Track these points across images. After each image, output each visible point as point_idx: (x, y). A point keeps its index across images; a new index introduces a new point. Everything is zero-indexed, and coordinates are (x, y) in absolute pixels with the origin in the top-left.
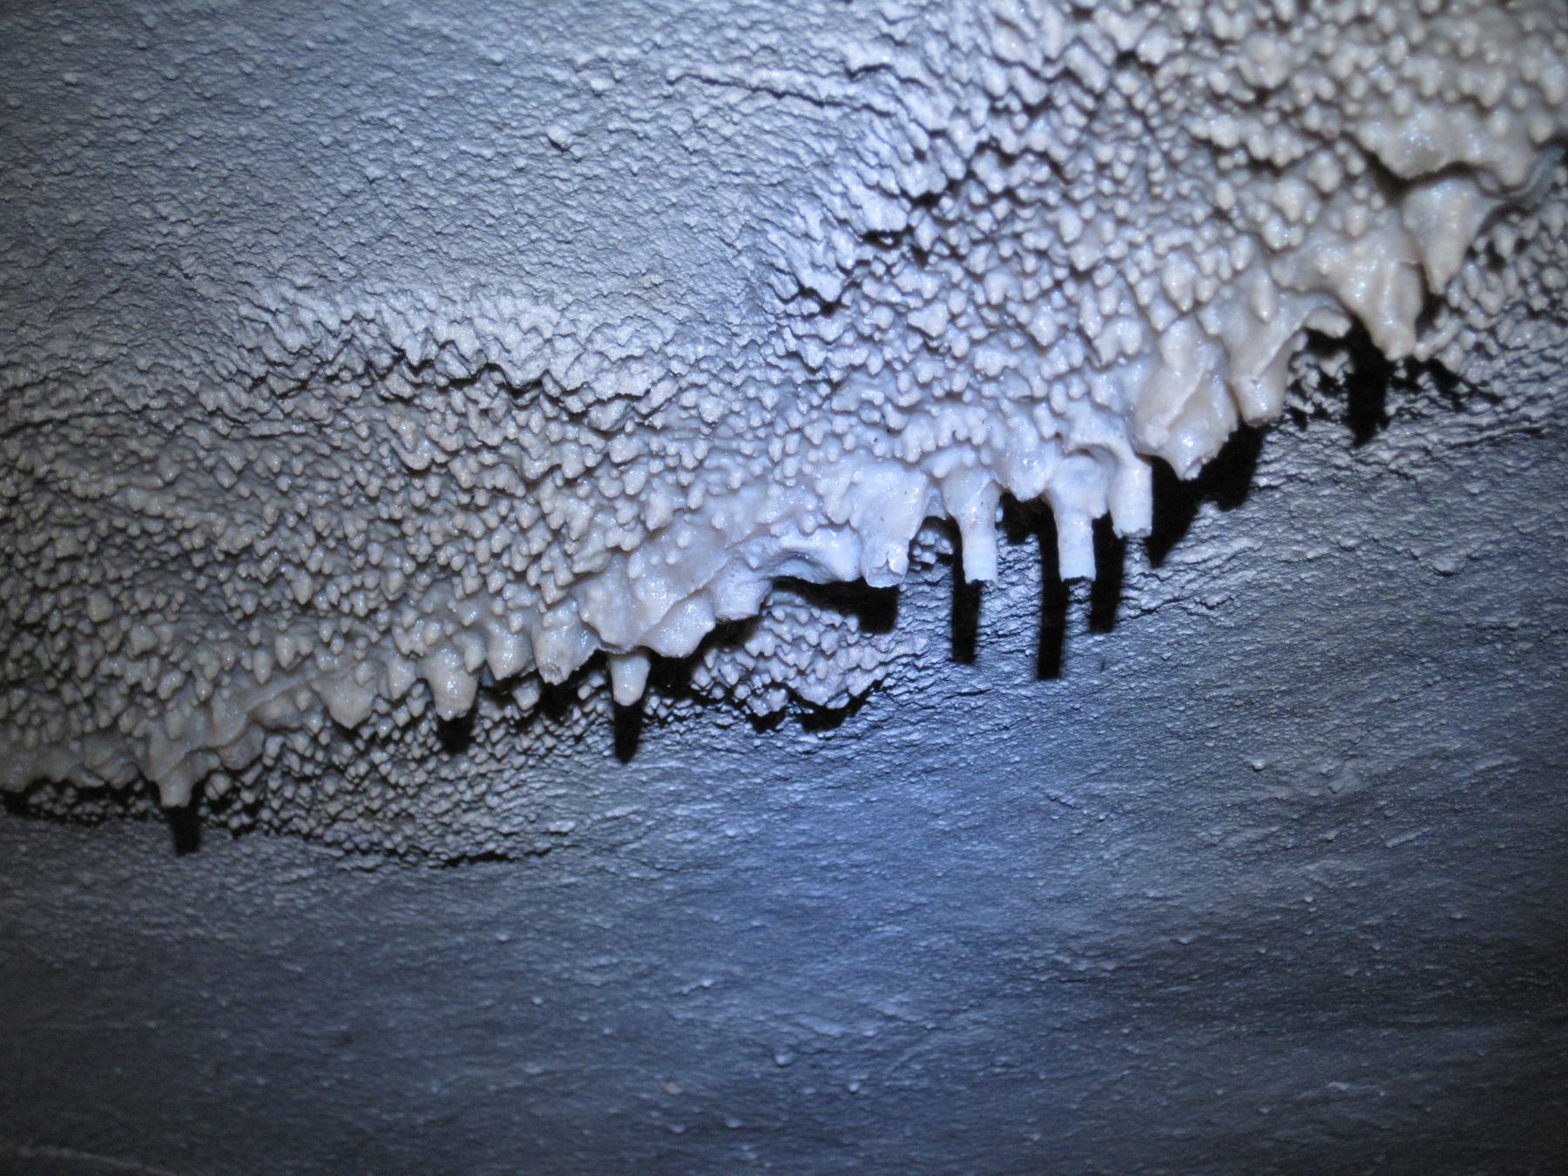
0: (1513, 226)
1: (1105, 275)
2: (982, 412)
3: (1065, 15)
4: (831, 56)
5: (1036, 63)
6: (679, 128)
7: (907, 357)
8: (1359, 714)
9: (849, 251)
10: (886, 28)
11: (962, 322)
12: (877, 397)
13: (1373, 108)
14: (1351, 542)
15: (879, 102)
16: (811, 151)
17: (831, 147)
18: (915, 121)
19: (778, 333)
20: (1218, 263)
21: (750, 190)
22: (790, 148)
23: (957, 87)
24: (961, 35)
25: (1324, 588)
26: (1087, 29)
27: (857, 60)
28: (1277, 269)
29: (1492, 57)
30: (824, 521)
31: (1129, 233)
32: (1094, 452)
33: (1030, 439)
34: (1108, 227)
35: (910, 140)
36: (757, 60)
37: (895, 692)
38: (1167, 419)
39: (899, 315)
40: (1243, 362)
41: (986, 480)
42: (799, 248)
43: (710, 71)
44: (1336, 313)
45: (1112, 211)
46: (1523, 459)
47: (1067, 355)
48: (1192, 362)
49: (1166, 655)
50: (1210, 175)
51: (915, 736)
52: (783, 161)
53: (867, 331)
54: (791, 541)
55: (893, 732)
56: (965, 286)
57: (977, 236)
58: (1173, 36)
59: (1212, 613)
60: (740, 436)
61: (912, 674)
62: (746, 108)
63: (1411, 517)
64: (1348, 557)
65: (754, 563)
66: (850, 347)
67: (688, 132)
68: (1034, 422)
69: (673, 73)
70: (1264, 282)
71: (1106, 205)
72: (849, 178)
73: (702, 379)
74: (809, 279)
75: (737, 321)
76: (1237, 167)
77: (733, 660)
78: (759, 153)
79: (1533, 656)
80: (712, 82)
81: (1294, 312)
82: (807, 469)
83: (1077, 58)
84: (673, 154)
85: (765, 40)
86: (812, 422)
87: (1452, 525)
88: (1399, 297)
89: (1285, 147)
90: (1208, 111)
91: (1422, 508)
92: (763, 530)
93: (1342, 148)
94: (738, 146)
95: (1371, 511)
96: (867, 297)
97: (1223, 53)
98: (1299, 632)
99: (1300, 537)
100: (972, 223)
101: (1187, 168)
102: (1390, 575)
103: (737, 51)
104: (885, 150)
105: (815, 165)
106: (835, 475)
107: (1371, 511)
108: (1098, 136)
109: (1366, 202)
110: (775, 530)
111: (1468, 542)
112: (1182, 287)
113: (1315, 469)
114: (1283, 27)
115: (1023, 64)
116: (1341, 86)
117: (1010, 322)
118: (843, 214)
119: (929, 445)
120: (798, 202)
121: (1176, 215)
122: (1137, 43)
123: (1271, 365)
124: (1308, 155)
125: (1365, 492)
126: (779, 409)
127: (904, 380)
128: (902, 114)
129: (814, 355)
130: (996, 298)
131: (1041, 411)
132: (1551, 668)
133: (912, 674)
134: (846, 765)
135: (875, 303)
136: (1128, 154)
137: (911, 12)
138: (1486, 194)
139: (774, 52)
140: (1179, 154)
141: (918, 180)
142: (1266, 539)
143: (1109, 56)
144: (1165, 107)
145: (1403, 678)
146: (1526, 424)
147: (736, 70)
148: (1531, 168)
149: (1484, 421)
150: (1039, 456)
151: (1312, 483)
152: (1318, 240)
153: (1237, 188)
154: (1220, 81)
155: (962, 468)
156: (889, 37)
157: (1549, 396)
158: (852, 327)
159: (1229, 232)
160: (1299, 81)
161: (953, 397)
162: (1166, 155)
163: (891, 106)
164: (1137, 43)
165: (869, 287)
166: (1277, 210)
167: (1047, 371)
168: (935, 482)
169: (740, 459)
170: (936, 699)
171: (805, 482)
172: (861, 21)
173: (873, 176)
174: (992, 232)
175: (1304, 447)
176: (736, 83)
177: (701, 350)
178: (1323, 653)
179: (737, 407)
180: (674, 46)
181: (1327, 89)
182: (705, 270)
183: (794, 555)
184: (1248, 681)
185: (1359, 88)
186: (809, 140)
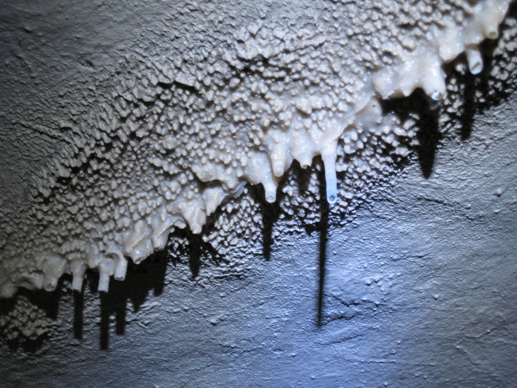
0: (232, 204)
1: (122, 202)
2: (84, 242)
3: (119, 119)
4: (56, 123)
5: (109, 131)
6: (13, 139)
7: (65, 220)
8: (187, 373)
9: (53, 183)
10: (71, 117)
11: (82, 212)
12: (56, 233)
13: (196, 161)
14: (186, 308)
15: (67, 139)
16: (47, 152)
17: (52, 151)
18: (75, 145)
19: (30, 208)
20: (153, 203)
21: (29, 162)
22: (42, 150)
23: (88, 136)
24: (90, 121)
25: (178, 323)
26: (123, 125)
27: (63, 124)
28: (168, 207)
29: (228, 151)
30: (35, 269)
31: (130, 191)
32: (114, 256)
33: (96, 252)
34: (124, 188)
35: (73, 150)
36: (36, 121)
37: (51, 339)
38: (133, 245)
39: (65, 207)
40: (156, 232)
41: (82, 263)
42: (40, 181)
43: (23, 122)
44: (182, 221)
45: (125, 183)
46: (236, 286)
47: (109, 226)
48: (142, 232)
49: (132, 340)
50: (153, 176)
51: (56, 359)
52: (39, 154)
53: (55, 210)
54: (25, 274)
55: (50, 356)
56: (84, 200)
57: (88, 184)
58: (147, 131)
59: (146, 327)
60: (15, 240)
61: (56, 333)
62: (32, 136)
63: (203, 302)
64: (185, 313)
65: (14, 280)
66: (50, 215)
67: (15, 141)
68: (98, 246)
69: (14, 121)
70: (164, 211)
71: (124, 181)
72: (56, 161)
73: (7, 219)
74: (41, 190)
75: (20, 202)
76: (160, 174)
77: (4, 318)
78: (33, 150)
79: (238, 360)
80: (23, 126)
81: (171, 220)
82: (33, 253)
83: (120, 132)
84: (10, 147)
85: (40, 115)
86: (37, 238)
87: (215, 307)
88: (199, 218)
89: (173, 170)
90: (154, 156)
91: (207, 299)
92: (18, 270)
93: (188, 172)
94: (28, 147)
95: (193, 298)
96: (57, 200)
97: (159, 139)
98: (171, 339)
99: (172, 304)
100: (87, 180)
101: (147, 173)
102: (198, 322)
103: (31, 118)
104: (66, 153)
105: (48, 156)
106: (40, 256)
107: (193, 298)
108: (124, 158)
109: (193, 190)
110: (21, 270)
111: (219, 314)
112: (142, 209)
113: (177, 280)
114: (175, 133)
115: (105, 132)
116: (189, 152)
117: (95, 213)
118: (53, 172)
119: (68, 250)
120: (42, 167)
121: (143, 188)
122: (136, 131)
123: (163, 233)
124: (179, 174)
125: (191, 290)
126: (28, 233)
127: (64, 228)
128: (73, 143)
129: (40, 215)
130: (91, 204)
131: (101, 243)
132: (244, 365)
133: (56, 333)
134: (34, 368)
135: (59, 202)
136: (131, 165)
137: (79, 113)
138: (225, 191)
139: (41, 120)
140: (145, 168)
141: (74, 163)
142: (162, 303)
143: (128, 133)
144: (143, 152)
145: (201, 361)
146: (236, 273)
147: (30, 123)
148: (236, 186)
149: (224, 269)
150: (98, 256)
151: (176, 285)
152: (180, 200)
153: (160, 181)
154: (157, 147)
155: (77, 259)
156: (72, 119)
157: (242, 264)
158: (51, 209)
159: (157, 195)
160: (178, 150)
161: (77, 236)
162: (142, 167)
163: (70, 141)
164: (136, 131)
165: (58, 197)
166: (170, 189)
167: (103, 230)
168: (69, 262)
169: (15, 248)
170: (63, 345)
171: (32, 257)
172: (65, 114)
173: (63, 161)
174: (93, 184)
175: (174, 271)
176: (29, 127)
177: (9, 210)
178: (178, 348)
179: (16, 230)
180: (15, 114)
181: (185, 153)
182: (14, 185)
183: (26, 280)
184: (156, 355)
185: (193, 154)
186: (47, 148)
